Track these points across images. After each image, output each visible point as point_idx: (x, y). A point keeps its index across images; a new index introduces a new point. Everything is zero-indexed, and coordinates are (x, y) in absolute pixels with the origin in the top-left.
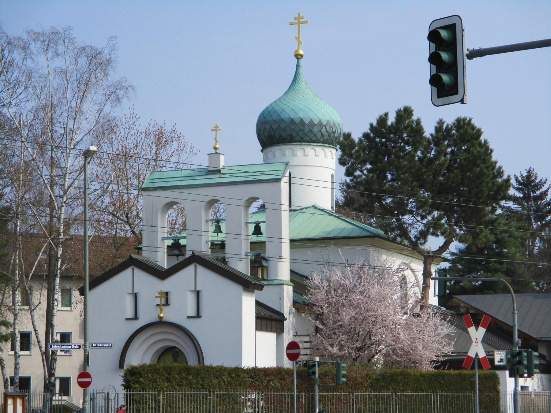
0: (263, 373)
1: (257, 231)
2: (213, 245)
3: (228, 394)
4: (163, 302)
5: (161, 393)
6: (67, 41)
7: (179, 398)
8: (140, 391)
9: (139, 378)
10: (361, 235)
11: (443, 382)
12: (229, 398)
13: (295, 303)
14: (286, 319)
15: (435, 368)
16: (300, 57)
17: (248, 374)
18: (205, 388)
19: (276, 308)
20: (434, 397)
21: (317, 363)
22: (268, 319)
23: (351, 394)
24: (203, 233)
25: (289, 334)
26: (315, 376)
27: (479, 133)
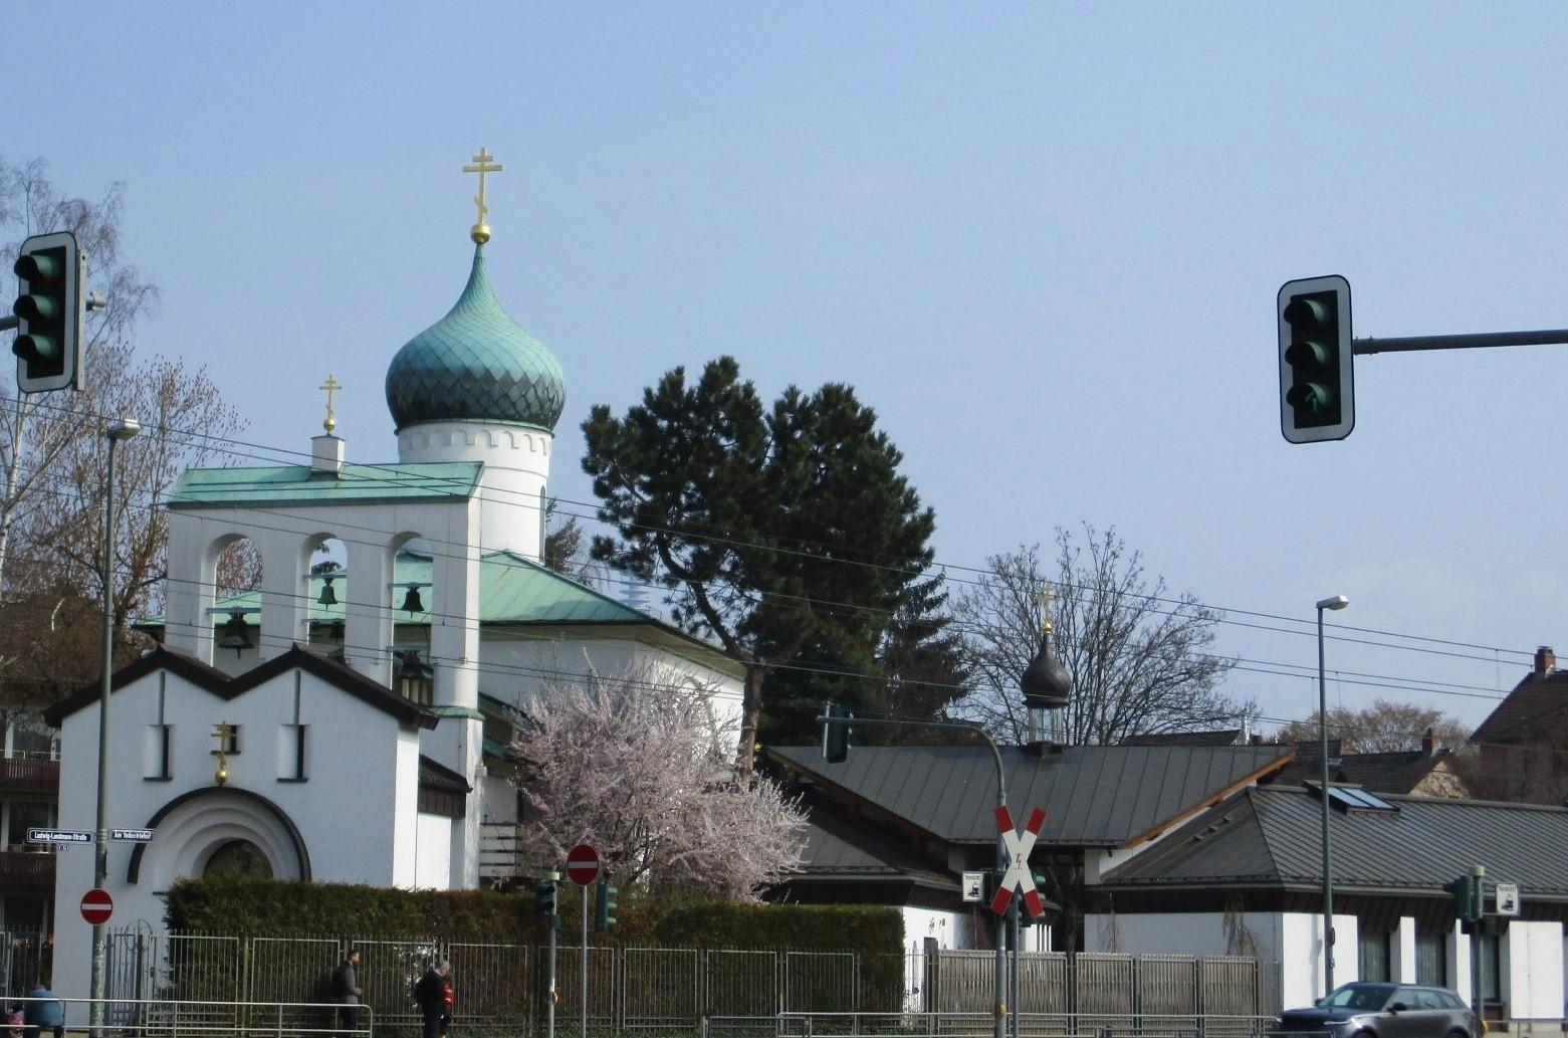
0: (448, 903)
1: (413, 602)
2: (316, 626)
3: (379, 945)
4: (227, 748)
5: (247, 939)
6: (33, 188)
7: (282, 950)
8: (204, 935)
9: (202, 907)
10: (617, 618)
11: (796, 928)
12: (379, 953)
13: (487, 756)
14: (470, 790)
15: (765, 897)
16: (482, 240)
17: (417, 904)
18: (331, 932)
19: (450, 764)
20: (778, 959)
21: (555, 885)
22: (441, 791)
23: (619, 950)
24: (298, 602)
25: (474, 820)
26: (551, 912)
27: (869, 418)
